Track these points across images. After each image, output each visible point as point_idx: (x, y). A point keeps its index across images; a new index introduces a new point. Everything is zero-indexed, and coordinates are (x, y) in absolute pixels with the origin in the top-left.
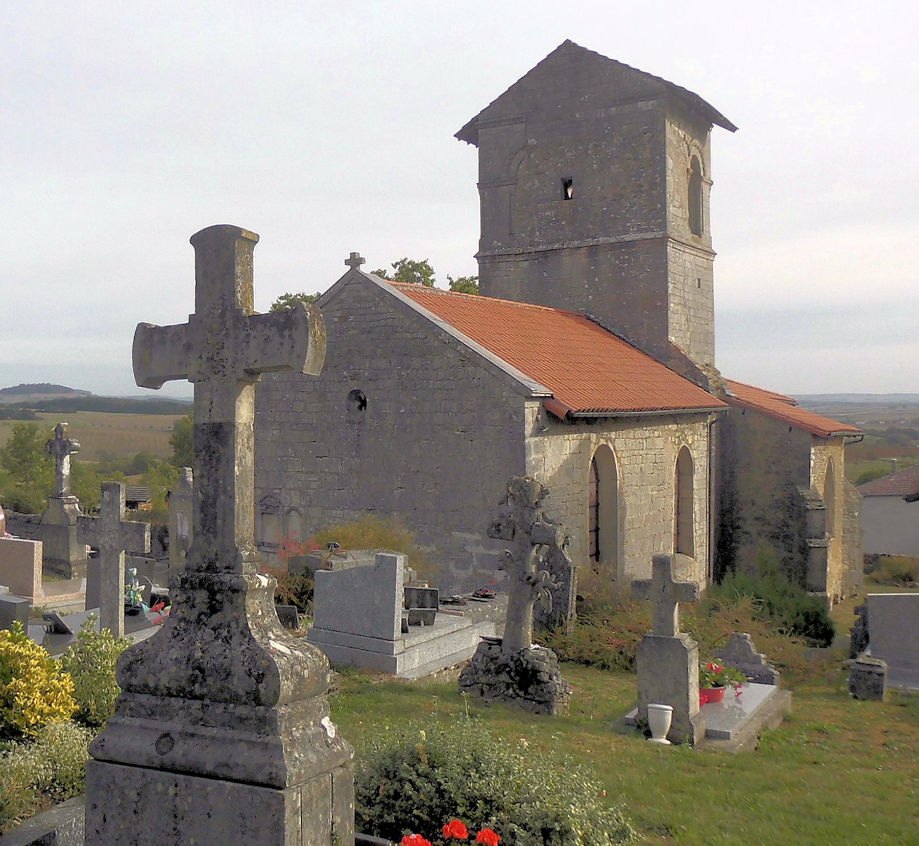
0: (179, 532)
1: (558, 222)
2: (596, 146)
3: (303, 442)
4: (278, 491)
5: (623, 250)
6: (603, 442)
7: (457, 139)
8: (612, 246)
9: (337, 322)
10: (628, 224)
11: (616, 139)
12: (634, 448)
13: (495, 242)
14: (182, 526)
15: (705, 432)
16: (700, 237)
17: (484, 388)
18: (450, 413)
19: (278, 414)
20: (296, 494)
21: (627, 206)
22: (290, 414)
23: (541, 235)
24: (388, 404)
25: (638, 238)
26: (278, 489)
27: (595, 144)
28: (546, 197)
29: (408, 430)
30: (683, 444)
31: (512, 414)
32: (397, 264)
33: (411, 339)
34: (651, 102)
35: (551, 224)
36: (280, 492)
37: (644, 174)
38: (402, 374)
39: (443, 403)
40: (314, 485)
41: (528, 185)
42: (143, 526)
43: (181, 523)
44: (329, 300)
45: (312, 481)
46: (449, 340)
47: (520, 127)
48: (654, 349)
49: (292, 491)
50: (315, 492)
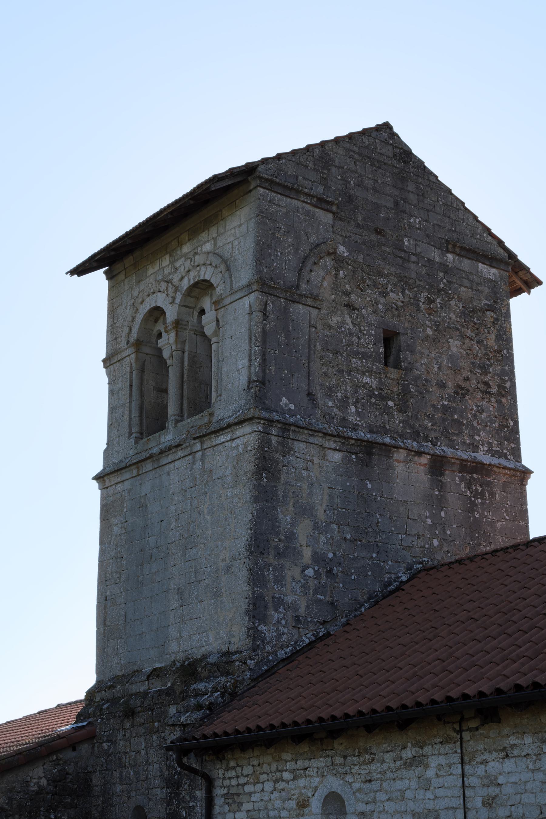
5: (475, 476)
13: (284, 400)
23: (358, 413)
28: (363, 350)
34: (493, 271)
35: (373, 400)
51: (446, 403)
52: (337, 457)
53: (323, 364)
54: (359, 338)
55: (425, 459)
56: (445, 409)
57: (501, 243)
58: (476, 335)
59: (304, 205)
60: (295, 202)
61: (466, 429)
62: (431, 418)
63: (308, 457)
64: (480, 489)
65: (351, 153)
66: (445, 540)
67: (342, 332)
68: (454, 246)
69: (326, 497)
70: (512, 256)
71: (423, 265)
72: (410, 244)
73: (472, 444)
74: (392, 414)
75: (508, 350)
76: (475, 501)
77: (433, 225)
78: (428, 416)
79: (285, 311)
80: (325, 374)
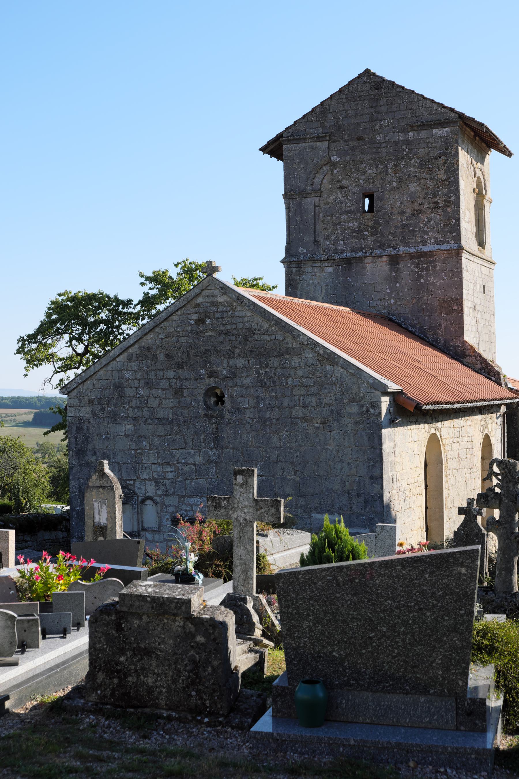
0: (97, 520)
1: (361, 232)
2: (396, 166)
3: (158, 436)
4: (132, 482)
5: (422, 259)
6: (433, 431)
7: (262, 153)
8: (412, 256)
9: (193, 324)
10: (426, 237)
11: (413, 160)
12: (453, 436)
13: (301, 249)
14: (99, 514)
15: (499, 421)
16: (484, 248)
17: (342, 384)
18: (309, 408)
19: (131, 409)
20: (151, 484)
21: (424, 221)
22: (144, 410)
23: (344, 244)
24: (247, 399)
25: (435, 249)
26: (132, 480)
27: (394, 164)
28: (349, 209)
29: (268, 423)
30: (486, 432)
31: (369, 407)
32: (178, 263)
33: (269, 341)
34: (445, 130)
35: (354, 234)
36: (134, 483)
37: (440, 193)
38: (261, 372)
39: (302, 398)
40: (170, 475)
41: (331, 198)
42: (280, 502)
43: (99, 511)
44: (185, 304)
45: (168, 472)
46: (307, 341)
47: (325, 145)
48: (451, 348)
49: (147, 482)
50: (172, 482)
51: (405, 222)
52: (330, 270)
53: (324, 224)
54: (346, 203)
55: (385, 259)
56: (403, 226)
57: (452, 110)
58: (430, 175)
59: (310, 143)
60: (304, 144)
61: (418, 234)
62: (394, 234)
63: (314, 274)
64: (425, 266)
65: (340, 100)
66: (398, 299)
67: (336, 203)
68: (412, 127)
69: (324, 291)
70: (461, 116)
71: (391, 147)
72: (381, 137)
73: (422, 241)
74: (367, 239)
75: (454, 177)
76: (421, 273)
77: (398, 119)
78: (391, 233)
79: (300, 204)
80: (325, 229)
